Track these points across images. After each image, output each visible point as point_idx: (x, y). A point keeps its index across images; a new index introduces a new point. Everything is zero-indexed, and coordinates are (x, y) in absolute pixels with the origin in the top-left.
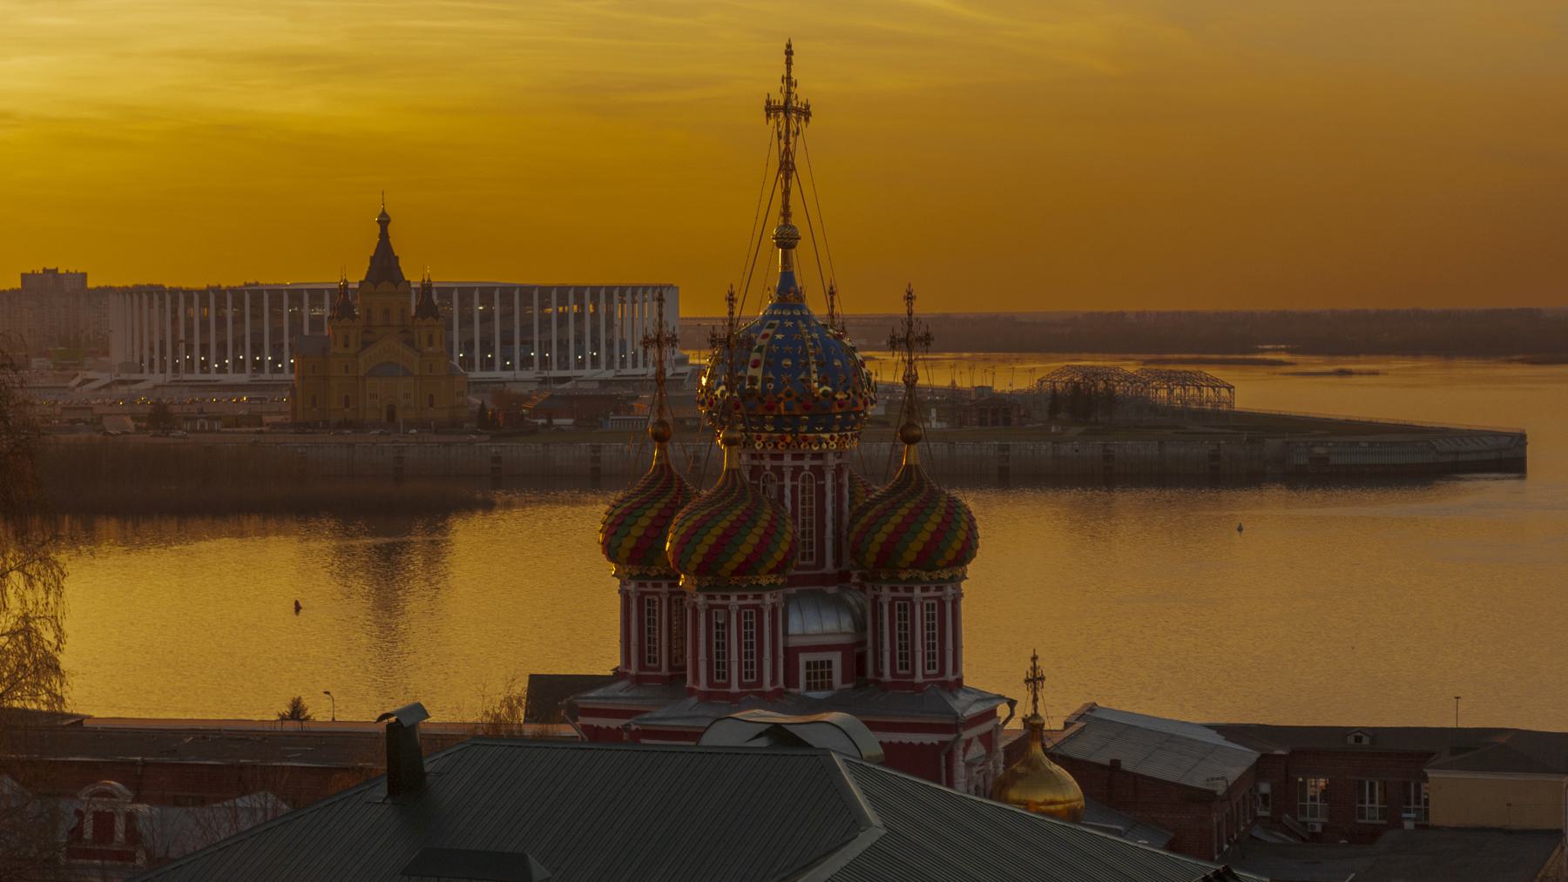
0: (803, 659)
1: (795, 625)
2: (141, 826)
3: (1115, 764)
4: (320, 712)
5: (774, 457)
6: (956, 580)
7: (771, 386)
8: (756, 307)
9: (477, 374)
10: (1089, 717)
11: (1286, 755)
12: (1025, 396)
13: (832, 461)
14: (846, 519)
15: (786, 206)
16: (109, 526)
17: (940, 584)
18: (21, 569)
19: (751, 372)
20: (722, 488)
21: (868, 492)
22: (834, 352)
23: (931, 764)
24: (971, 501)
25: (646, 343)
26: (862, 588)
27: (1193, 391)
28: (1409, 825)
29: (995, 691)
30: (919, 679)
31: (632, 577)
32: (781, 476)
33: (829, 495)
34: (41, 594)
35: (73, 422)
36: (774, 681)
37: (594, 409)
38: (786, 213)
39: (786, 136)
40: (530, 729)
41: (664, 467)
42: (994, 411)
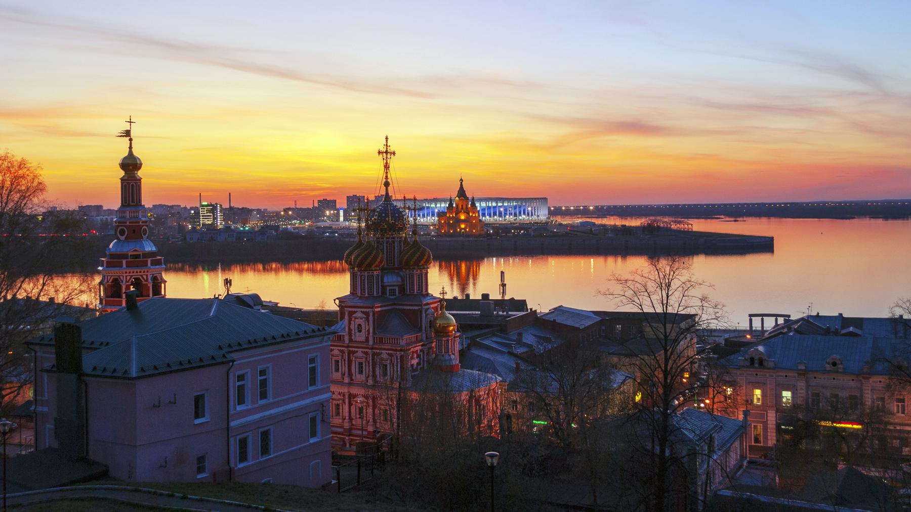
0: (388, 288)
1: (385, 280)
12: (636, 227)
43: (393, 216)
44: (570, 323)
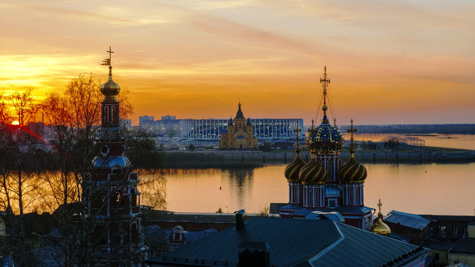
0: (329, 200)
1: (327, 193)
2: (185, 236)
3: (398, 223)
4: (225, 212)
5: (322, 156)
6: (362, 183)
7: (322, 140)
8: (318, 123)
9: (260, 138)
10: (394, 213)
11: (436, 222)
13: (335, 157)
14: (338, 170)
15: (325, 102)
16: (180, 171)
17: (359, 184)
18: (157, 180)
19: (317, 137)
20: (296, 161)
21: (343, 164)
22: (335, 133)
23: (357, 223)
24: (367, 166)
25: (294, 131)
26: (342, 185)
27: (416, 142)
28: (464, 237)
29: (371, 207)
30: (354, 204)
31: (291, 182)
32: (324, 160)
33: (334, 165)
34: (161, 185)
35: (173, 148)
36: (322, 205)
37: (285, 146)
38: (325, 103)
39: (325, 86)
40: (270, 215)
41: (298, 158)
42: (372, 146)
43: (334, 138)
44: (408, 224)
